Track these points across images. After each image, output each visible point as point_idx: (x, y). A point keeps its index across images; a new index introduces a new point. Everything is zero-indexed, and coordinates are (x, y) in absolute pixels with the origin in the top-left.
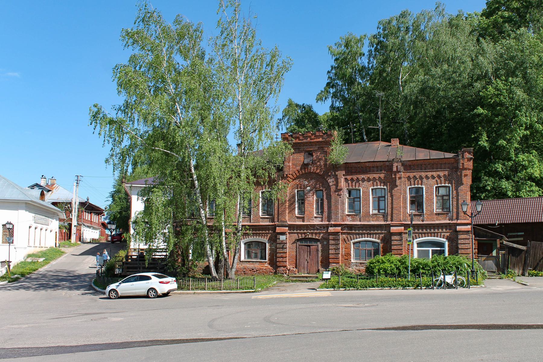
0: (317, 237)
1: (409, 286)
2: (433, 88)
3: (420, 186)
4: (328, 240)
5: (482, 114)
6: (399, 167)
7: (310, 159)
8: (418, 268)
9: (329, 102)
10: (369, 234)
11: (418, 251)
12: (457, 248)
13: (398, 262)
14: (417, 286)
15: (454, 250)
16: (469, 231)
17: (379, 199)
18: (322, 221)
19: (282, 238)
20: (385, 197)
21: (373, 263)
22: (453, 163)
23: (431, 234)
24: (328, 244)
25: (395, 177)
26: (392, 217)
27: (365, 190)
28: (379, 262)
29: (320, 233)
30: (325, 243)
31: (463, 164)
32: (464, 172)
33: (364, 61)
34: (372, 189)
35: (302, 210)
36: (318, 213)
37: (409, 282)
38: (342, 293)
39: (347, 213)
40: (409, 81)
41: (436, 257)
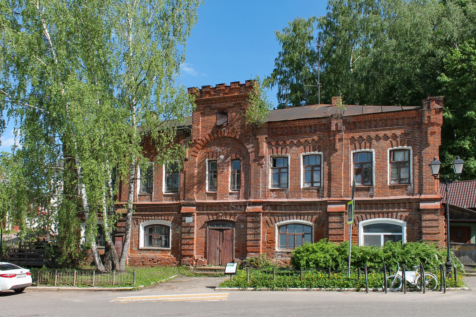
0: (228, 219)
1: (348, 286)
2: (386, 61)
3: (368, 150)
4: (245, 222)
5: (446, 82)
6: (339, 124)
7: (223, 119)
8: (363, 260)
9: (276, 88)
10: (299, 215)
11: (365, 236)
12: (421, 233)
13: (335, 251)
14: (361, 286)
15: (416, 235)
16: (437, 209)
17: (312, 169)
18: (238, 198)
19: (188, 220)
20: (320, 166)
21: (299, 253)
22: (415, 118)
23: (383, 214)
24: (246, 228)
25: (334, 139)
26: (329, 191)
27: (295, 157)
28: (308, 250)
29: (235, 214)
30: (242, 226)
31: (429, 117)
32: (430, 130)
33: (313, 46)
34: (304, 157)
35: (213, 186)
36: (233, 188)
37: (348, 279)
38: (250, 295)
39: (270, 187)
40: (358, 56)
41: (391, 244)
